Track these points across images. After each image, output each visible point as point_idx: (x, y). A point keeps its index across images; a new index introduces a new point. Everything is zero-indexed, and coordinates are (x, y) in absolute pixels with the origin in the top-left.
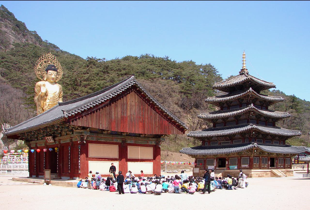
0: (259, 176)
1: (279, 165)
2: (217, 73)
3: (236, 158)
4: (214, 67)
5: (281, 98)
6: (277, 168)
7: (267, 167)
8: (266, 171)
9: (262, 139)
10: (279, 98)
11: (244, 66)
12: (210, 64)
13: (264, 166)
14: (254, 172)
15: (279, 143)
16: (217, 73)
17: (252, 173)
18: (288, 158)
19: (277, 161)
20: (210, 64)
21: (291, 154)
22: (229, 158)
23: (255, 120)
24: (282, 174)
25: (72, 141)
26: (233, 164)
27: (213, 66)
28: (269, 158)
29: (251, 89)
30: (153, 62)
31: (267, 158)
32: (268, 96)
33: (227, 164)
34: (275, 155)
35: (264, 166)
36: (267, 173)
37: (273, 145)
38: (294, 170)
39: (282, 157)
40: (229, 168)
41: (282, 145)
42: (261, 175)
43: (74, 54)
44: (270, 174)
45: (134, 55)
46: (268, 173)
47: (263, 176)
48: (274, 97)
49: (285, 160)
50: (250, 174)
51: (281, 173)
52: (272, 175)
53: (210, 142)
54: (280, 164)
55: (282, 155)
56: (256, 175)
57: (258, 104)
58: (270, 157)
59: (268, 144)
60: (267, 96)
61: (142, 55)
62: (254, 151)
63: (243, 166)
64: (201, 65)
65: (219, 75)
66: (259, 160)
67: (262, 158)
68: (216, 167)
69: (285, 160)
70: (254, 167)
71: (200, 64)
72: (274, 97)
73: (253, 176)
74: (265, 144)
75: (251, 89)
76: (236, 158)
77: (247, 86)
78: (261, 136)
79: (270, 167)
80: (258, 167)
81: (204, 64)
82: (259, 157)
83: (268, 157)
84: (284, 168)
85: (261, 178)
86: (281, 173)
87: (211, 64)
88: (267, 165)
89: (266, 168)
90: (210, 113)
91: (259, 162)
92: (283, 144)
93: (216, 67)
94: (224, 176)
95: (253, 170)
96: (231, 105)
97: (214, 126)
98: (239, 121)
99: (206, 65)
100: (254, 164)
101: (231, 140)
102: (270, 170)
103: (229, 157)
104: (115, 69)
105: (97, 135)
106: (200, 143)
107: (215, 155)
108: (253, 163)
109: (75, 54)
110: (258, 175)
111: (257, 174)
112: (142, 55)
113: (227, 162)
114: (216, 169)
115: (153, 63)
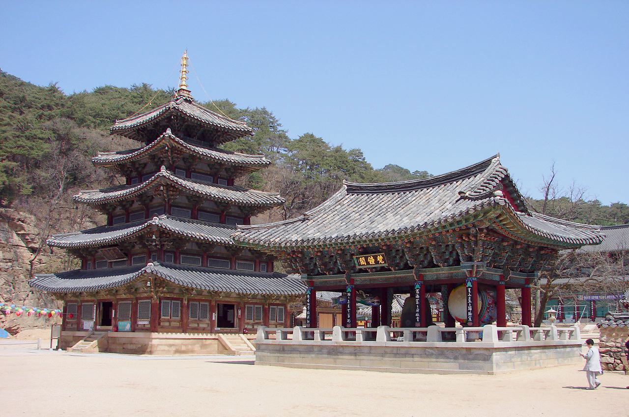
0: (178, 351)
1: (248, 324)
2: (279, 128)
3: (129, 302)
4: (272, 116)
5: (264, 159)
6: (240, 330)
7: (209, 328)
8: (202, 339)
9: (199, 255)
10: (258, 160)
11: (184, 83)
12: (264, 108)
13: (198, 325)
14: (158, 339)
15: (255, 267)
16: (279, 128)
17: (155, 342)
18: (278, 305)
19: (240, 312)
20: (264, 108)
21: (285, 296)
22: (118, 302)
23: (188, 208)
24: (248, 346)
25: (497, 294)
26: (124, 319)
27: (271, 114)
28: (213, 303)
29: (169, 131)
30: (141, 97)
31: (207, 303)
32: (235, 153)
33: (113, 316)
34: (235, 296)
35: (198, 325)
36: (204, 343)
37: (178, 265)
38: (580, 346)
39: (256, 303)
40: (117, 330)
41: (264, 272)
42: (183, 348)
43: (29, 82)
44: (217, 346)
45: (120, 85)
46: (211, 344)
47: (192, 351)
48: (248, 155)
49: (266, 312)
50: (150, 345)
51: (245, 343)
52: (221, 348)
53: (94, 262)
54: (252, 321)
55: (205, 293)
56: (166, 348)
57: (204, 172)
58: (216, 301)
59: (216, 268)
60: (232, 153)
61: (134, 86)
62: (146, 283)
63: (140, 323)
64: (246, 111)
65: (283, 131)
66: (180, 308)
67: (190, 303)
68: (96, 324)
69: (266, 312)
70: (163, 327)
71: (244, 108)
72: (248, 155)
73: (158, 349)
74: (209, 269)
75: (169, 131)
76: (129, 302)
77: (175, 127)
78: (168, 246)
79: (219, 329)
80: (178, 328)
81: (252, 108)
82: (179, 302)
83: (210, 301)
84: (184, 331)
85: (184, 356)
86: (245, 343)
87: (267, 110)
88: (207, 321)
89: (203, 331)
90: (102, 191)
91: (182, 313)
92: (267, 272)
93: (276, 115)
94: (106, 347)
95: (155, 335)
96: (145, 173)
97: (110, 222)
98: (151, 210)
99: (255, 109)
100: (162, 317)
101: (126, 255)
102: (213, 336)
103: (245, 303)
104: (39, 105)
105: (175, 262)
106: (77, 264)
107: (94, 292)
108: (160, 317)
109: (32, 83)
110: (173, 348)
111: (171, 345)
112: (134, 86)
113: (114, 311)
114: (96, 330)
115: (142, 99)
